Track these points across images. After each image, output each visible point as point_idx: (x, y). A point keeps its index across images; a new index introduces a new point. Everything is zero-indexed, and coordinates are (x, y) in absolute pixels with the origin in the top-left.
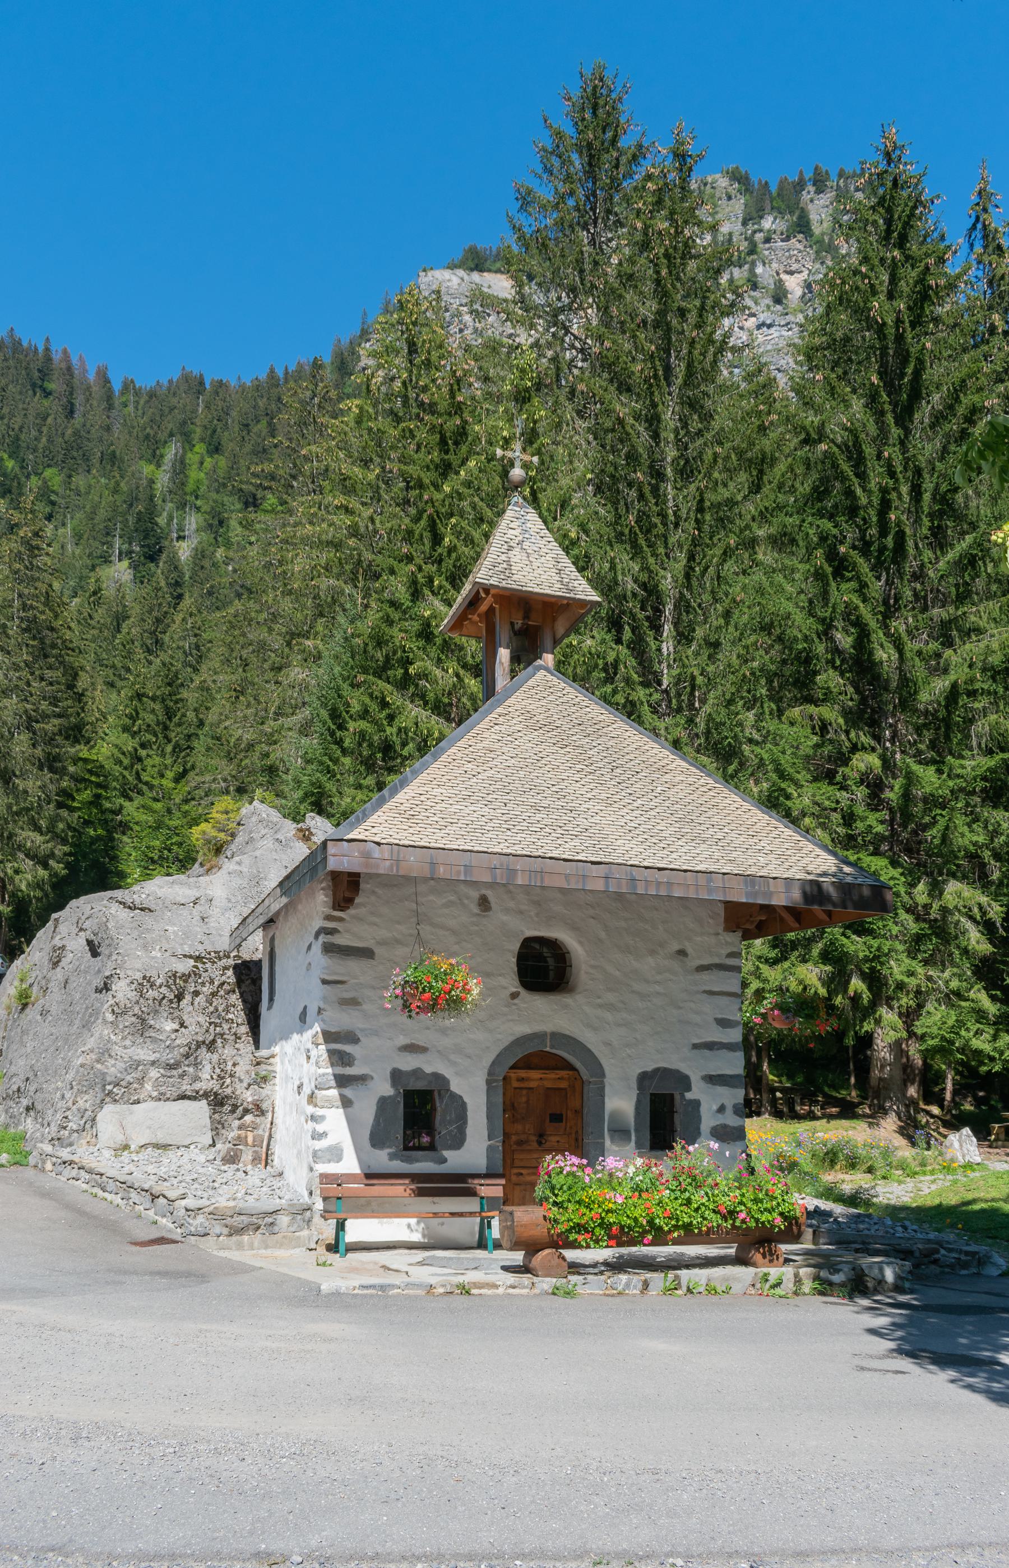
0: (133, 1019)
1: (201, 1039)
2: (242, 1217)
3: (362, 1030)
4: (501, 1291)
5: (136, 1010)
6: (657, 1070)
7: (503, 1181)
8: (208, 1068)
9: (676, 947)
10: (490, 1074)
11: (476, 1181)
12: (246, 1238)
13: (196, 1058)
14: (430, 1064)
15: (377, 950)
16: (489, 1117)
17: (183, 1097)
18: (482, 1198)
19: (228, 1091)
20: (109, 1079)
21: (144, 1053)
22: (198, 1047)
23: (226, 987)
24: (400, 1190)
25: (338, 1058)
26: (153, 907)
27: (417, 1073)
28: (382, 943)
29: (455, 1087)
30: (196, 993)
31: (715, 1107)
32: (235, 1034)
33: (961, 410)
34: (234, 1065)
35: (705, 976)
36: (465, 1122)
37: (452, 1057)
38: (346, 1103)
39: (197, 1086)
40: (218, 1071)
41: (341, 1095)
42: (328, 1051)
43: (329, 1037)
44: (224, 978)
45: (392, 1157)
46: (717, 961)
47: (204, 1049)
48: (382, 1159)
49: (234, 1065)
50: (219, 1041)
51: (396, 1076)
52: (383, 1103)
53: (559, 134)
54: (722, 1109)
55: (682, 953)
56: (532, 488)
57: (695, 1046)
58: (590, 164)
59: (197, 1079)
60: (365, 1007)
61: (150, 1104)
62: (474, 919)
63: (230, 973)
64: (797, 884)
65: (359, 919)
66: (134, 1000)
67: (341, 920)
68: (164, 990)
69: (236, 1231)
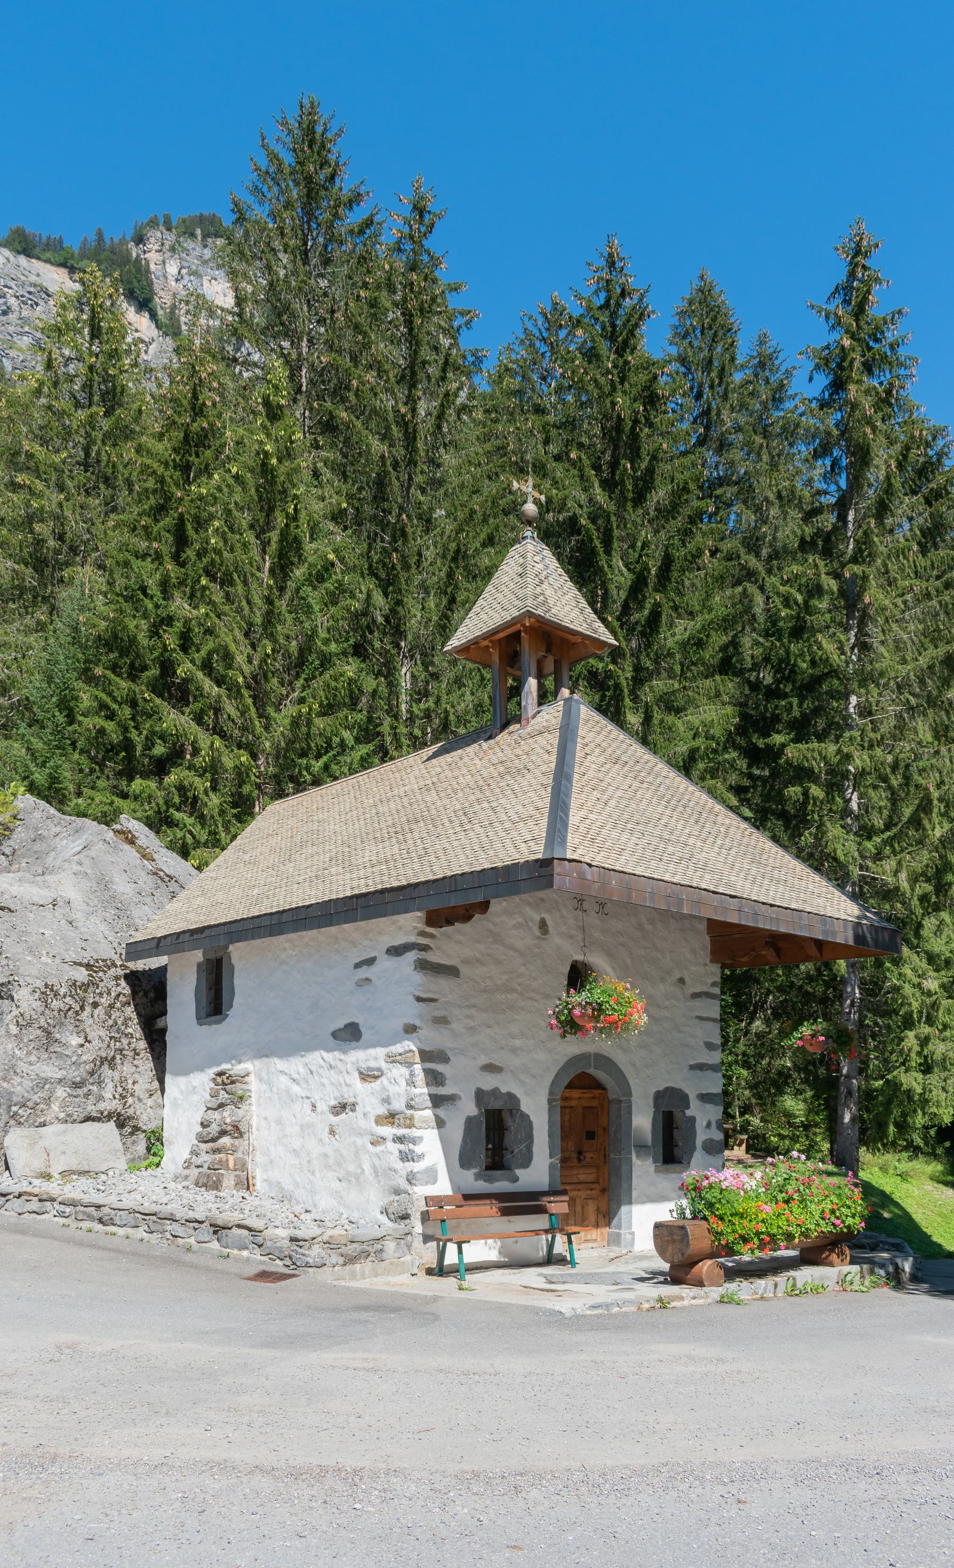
0: (39, 1032)
1: (104, 1055)
2: (355, 1245)
3: (451, 1049)
4: (686, 1303)
5: (42, 1022)
6: (667, 1089)
7: (566, 1198)
8: (110, 1086)
9: (678, 976)
10: (551, 1093)
11: (546, 1199)
12: (358, 1266)
13: (100, 1076)
14: (506, 1085)
15: (463, 969)
16: (550, 1135)
17: (89, 1119)
18: (551, 1215)
19: (130, 1112)
20: (15, 1099)
21: (50, 1070)
22: (102, 1064)
23: (122, 998)
24: (489, 1209)
25: (434, 1078)
26: (12, 907)
27: (495, 1092)
28: (466, 962)
29: (524, 1107)
30: (95, 1005)
31: (705, 1124)
32: (134, 1050)
33: (686, 511)
34: (134, 1083)
35: (698, 1003)
36: (532, 1142)
37: (522, 1077)
38: (440, 1123)
39: (102, 1106)
40: (120, 1089)
41: (437, 1117)
42: (424, 1070)
43: (425, 1056)
44: (119, 989)
45: (478, 1177)
46: (705, 989)
47: (106, 1066)
48: (471, 1180)
49: (134, 1083)
50: (118, 1057)
51: (480, 1095)
52: (469, 1121)
53: (273, 157)
54: (709, 1125)
55: (682, 981)
56: (296, 506)
57: (692, 1067)
58: (308, 196)
59: (100, 1098)
60: (453, 1026)
61: (58, 1127)
62: (536, 942)
63: (123, 983)
64: (850, 926)
65: (448, 937)
66: (40, 1009)
67: (432, 936)
68: (68, 999)
69: (350, 1260)
